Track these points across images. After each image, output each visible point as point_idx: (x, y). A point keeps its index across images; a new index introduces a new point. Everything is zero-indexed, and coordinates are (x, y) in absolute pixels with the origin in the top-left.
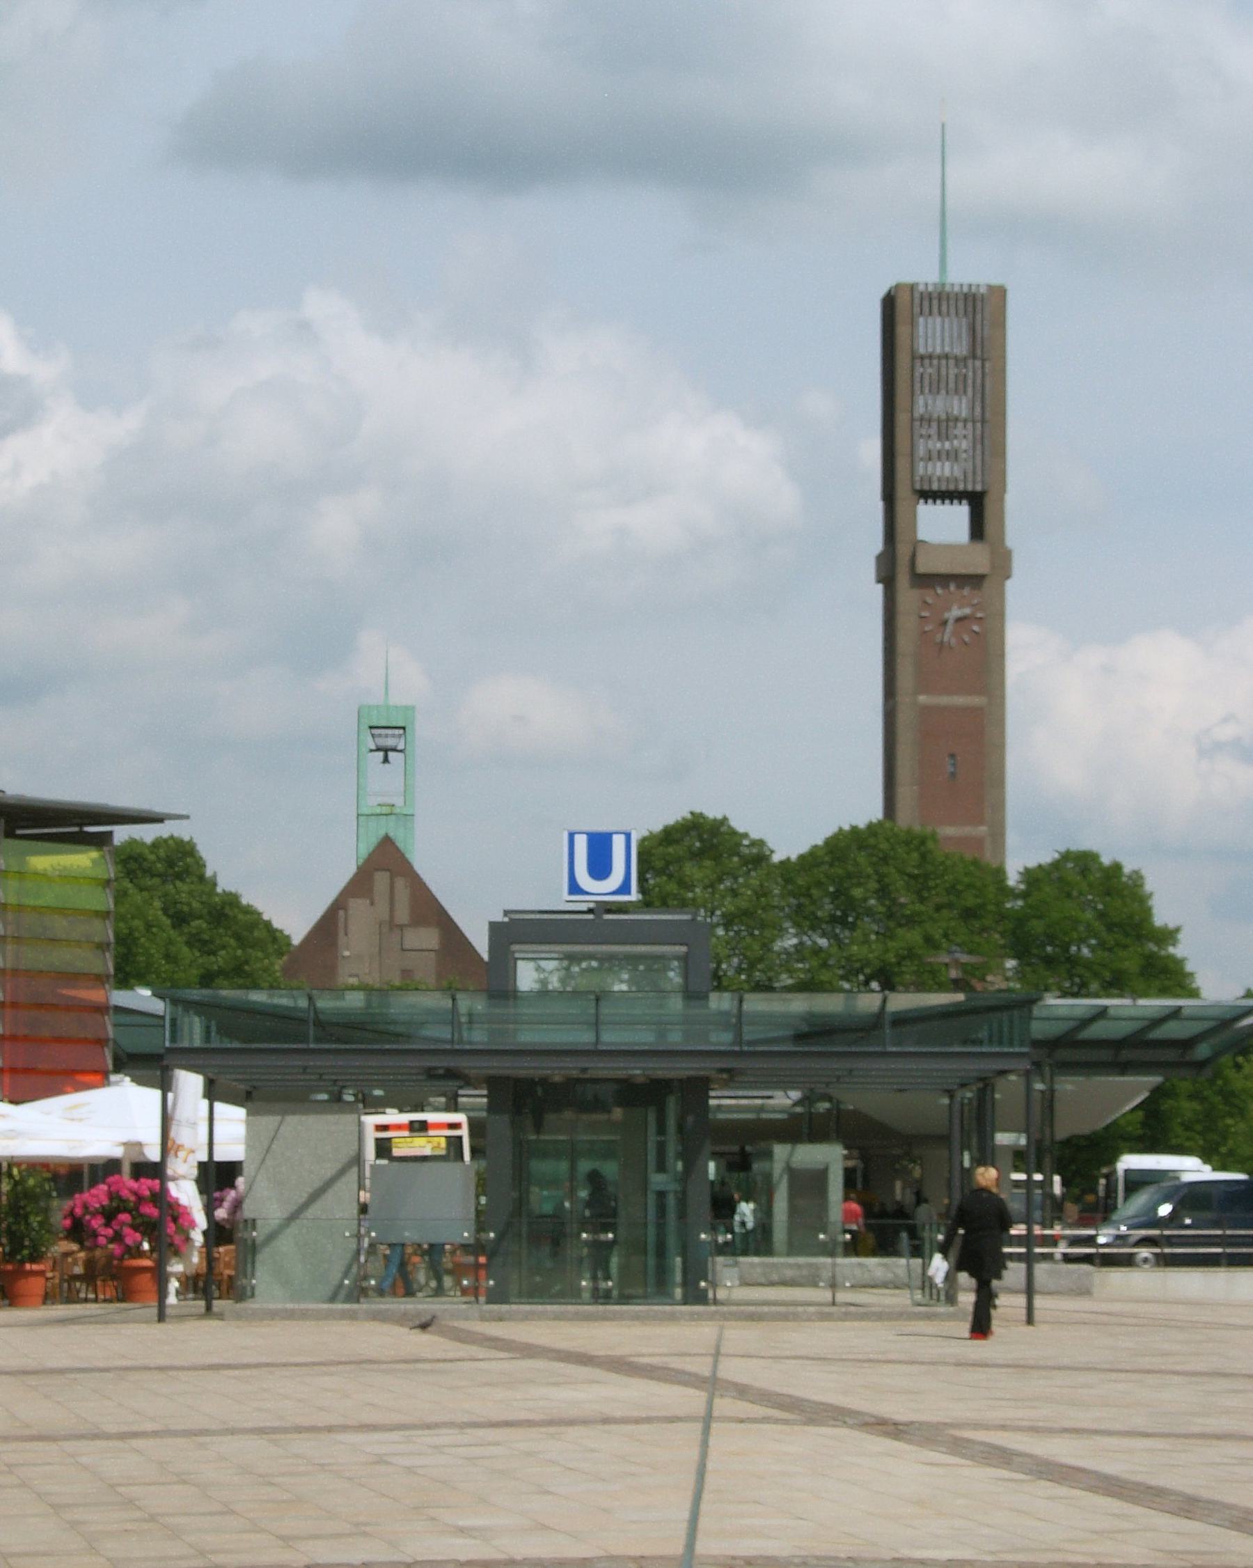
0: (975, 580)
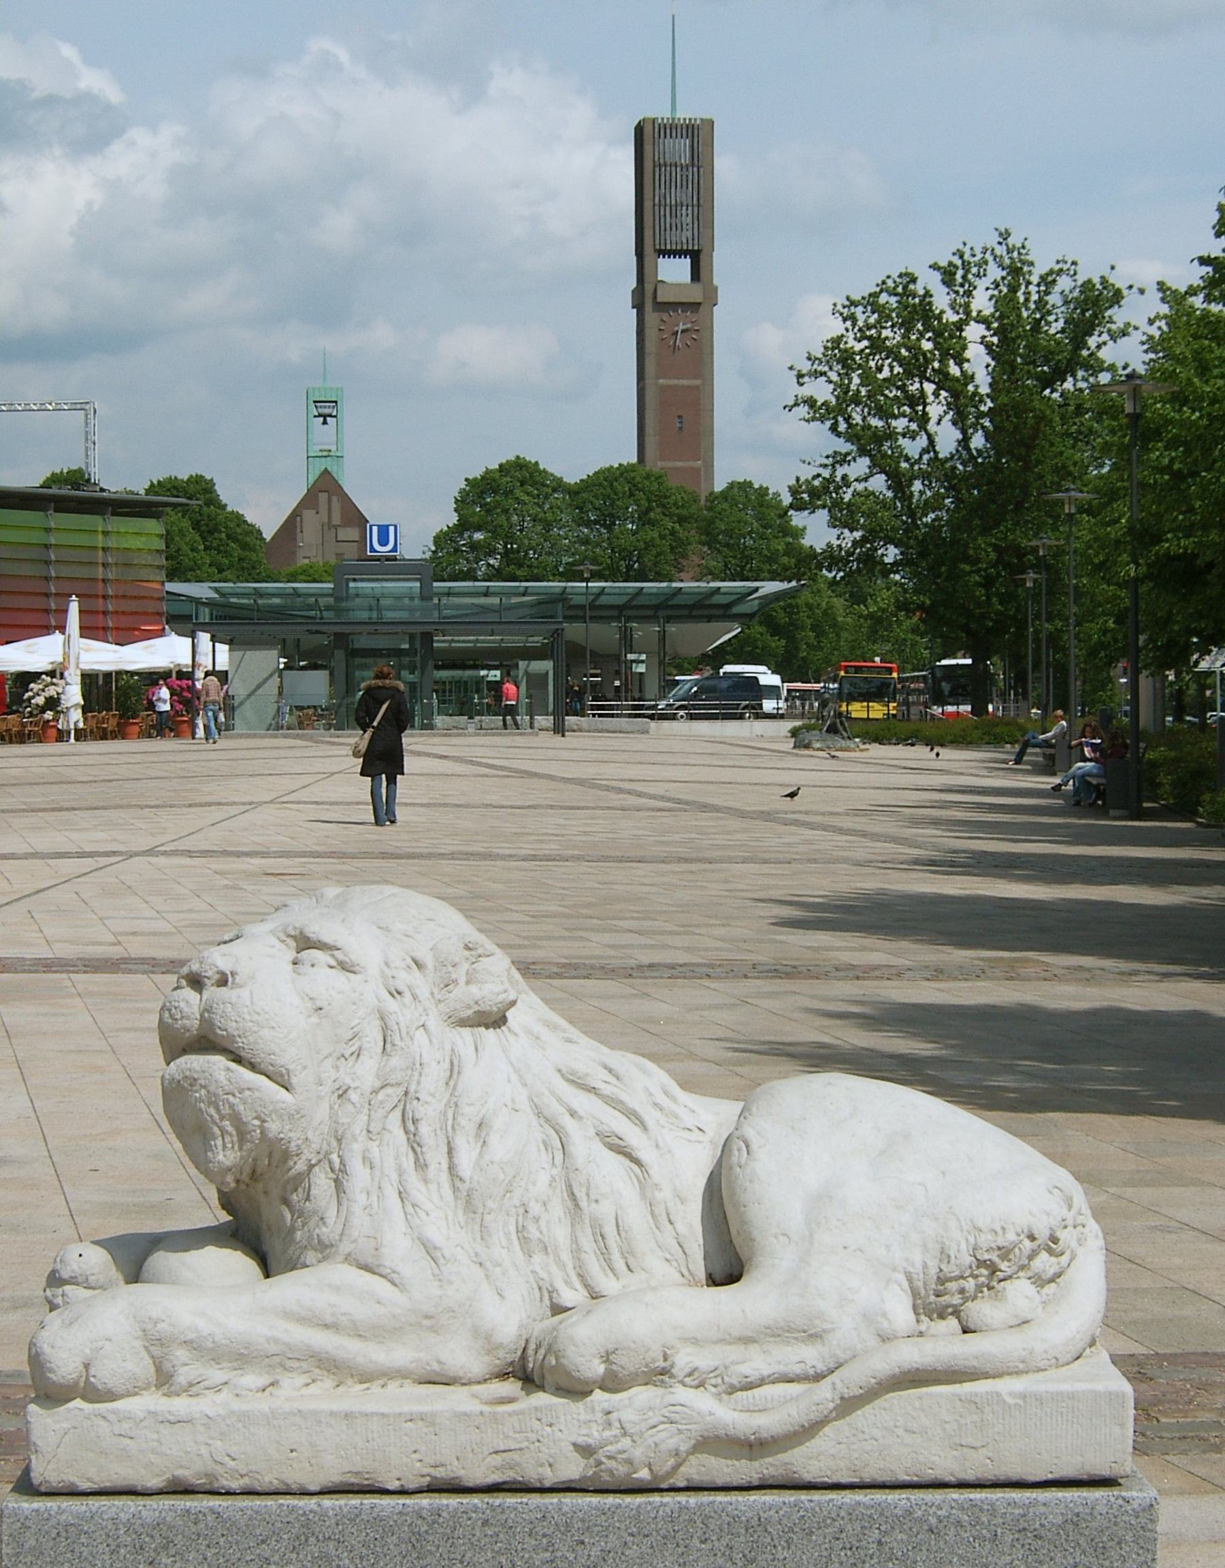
0: (694, 306)
